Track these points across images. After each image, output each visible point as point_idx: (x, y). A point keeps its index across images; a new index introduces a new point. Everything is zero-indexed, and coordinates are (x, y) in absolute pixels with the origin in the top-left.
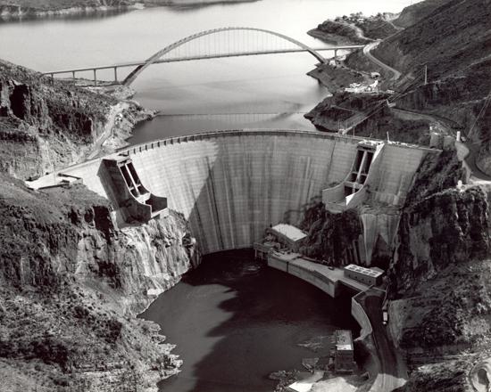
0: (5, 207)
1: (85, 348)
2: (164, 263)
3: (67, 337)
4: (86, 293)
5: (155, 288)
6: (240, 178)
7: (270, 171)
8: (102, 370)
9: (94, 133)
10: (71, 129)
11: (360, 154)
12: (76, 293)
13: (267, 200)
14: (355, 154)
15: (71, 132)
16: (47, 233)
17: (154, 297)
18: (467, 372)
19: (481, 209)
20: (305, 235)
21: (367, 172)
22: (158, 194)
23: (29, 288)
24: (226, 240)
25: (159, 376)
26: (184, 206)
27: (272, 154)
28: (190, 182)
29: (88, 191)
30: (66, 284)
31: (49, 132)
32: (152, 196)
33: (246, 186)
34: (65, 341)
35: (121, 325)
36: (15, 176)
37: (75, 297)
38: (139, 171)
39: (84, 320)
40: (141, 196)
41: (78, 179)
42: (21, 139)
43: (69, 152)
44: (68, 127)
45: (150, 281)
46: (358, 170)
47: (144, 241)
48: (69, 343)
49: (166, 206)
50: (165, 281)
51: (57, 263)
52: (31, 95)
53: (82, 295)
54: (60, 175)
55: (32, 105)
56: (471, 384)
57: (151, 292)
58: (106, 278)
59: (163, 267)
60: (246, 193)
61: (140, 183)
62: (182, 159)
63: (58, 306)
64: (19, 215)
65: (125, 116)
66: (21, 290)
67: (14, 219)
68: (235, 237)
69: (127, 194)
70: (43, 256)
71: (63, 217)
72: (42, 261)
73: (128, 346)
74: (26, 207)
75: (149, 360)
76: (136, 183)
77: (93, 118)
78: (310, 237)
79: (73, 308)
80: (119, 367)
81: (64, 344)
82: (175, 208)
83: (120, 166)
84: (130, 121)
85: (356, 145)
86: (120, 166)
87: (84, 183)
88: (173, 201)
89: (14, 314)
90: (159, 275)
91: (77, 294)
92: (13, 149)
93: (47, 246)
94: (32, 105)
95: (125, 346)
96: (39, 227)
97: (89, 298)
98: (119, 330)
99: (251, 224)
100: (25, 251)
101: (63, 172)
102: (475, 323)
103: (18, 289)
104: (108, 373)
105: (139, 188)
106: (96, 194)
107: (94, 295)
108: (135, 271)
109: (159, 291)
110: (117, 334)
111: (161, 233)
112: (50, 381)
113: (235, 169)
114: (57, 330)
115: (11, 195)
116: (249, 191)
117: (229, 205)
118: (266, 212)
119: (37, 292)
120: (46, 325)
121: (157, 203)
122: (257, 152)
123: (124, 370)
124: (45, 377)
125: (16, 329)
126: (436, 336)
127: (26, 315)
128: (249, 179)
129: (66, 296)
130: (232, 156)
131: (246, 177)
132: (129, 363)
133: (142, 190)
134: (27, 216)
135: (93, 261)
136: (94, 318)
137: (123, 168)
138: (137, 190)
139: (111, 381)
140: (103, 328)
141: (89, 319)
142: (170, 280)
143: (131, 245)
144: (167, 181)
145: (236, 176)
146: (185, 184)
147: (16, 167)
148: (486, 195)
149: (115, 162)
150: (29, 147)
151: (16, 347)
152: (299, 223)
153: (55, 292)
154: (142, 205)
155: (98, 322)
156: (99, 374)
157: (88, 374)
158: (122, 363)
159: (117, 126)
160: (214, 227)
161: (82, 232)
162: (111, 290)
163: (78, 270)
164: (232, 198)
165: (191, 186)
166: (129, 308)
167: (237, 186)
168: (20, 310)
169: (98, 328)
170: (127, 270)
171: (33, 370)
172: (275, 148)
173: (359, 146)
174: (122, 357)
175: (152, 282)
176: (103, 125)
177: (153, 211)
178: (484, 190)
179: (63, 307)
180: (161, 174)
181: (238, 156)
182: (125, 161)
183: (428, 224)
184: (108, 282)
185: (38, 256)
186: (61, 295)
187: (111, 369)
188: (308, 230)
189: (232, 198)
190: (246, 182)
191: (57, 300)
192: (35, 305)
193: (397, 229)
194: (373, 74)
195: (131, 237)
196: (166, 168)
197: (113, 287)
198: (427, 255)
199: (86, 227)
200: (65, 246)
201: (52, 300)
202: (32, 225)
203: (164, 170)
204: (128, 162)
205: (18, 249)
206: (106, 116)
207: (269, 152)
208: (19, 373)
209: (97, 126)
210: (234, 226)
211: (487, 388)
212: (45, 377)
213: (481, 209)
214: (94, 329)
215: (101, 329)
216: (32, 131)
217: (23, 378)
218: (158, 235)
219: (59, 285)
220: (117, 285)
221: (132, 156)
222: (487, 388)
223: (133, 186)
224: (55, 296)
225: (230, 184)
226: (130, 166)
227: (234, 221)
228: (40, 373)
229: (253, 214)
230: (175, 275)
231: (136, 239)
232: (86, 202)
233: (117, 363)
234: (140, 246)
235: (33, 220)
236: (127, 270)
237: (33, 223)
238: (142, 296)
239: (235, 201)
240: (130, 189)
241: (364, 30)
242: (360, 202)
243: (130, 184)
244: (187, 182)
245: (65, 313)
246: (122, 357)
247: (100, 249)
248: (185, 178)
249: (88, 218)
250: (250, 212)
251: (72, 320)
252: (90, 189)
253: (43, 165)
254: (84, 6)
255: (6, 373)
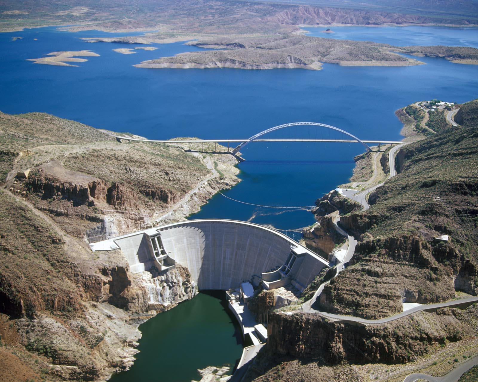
21: (291, 267)
26: (188, 264)
32: (168, 257)
38: (163, 240)
46: (287, 264)
55: (118, 195)
61: (163, 248)
71: (98, 271)
76: (160, 248)
81: (57, 349)
94: (118, 195)
96: (72, 281)
133: (163, 252)
140: (92, 339)
223: (157, 250)
242: (95, 367)
254: (278, 63)
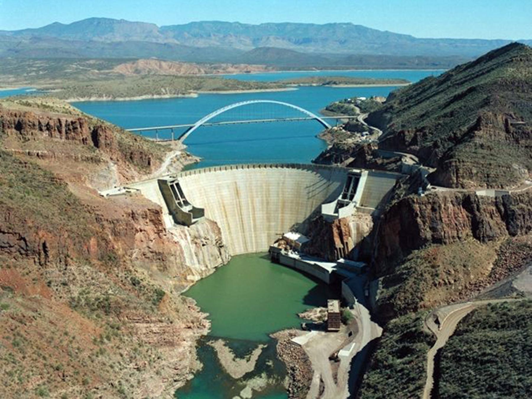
0: (81, 205)
1: (135, 305)
2: (201, 257)
3: (122, 296)
4: (140, 270)
5: (193, 275)
6: (260, 198)
7: (283, 194)
8: (148, 322)
9: (153, 168)
10: (135, 163)
11: (350, 179)
12: (131, 268)
13: (280, 215)
14: (346, 179)
15: (135, 165)
16: (112, 225)
17: (193, 281)
18: (424, 318)
19: (438, 209)
20: (308, 240)
22: (198, 206)
23: (95, 261)
24: (249, 244)
25: (192, 333)
27: (284, 181)
28: (222, 200)
29: (145, 198)
30: (124, 261)
31: (118, 160)
32: (193, 207)
33: (265, 204)
34: (120, 298)
35: (164, 293)
36: (90, 186)
37: (131, 271)
39: (137, 288)
40: (184, 207)
41: (138, 190)
42: (97, 161)
43: (133, 177)
44: (133, 162)
45: (190, 269)
46: (348, 191)
47: (186, 239)
48: (123, 300)
49: (203, 215)
50: (201, 270)
51: (119, 247)
52: (105, 132)
53: (137, 271)
54: (124, 188)
56: (426, 324)
57: (189, 278)
58: (156, 264)
59: (200, 260)
60: (265, 209)
61: (184, 197)
62: (217, 183)
63: (117, 276)
64: (91, 212)
65: (178, 160)
66: (90, 263)
67: (88, 214)
68: (257, 242)
69: (174, 205)
70: (108, 240)
71: (125, 215)
72: (107, 242)
73: (169, 309)
74: (98, 207)
75: (185, 320)
76: (182, 197)
77: (153, 156)
78: (312, 240)
79: (129, 279)
80: (161, 321)
82: (211, 218)
83: (169, 184)
84: (181, 163)
85: (347, 173)
86: (169, 184)
87: (142, 193)
88: (209, 213)
89: (83, 278)
90: (197, 266)
91: (133, 270)
92: (90, 168)
93: (112, 235)
95: (167, 308)
97: (141, 273)
98: (163, 296)
99: (268, 233)
100: (94, 235)
101: (127, 186)
102: (434, 292)
103: (88, 261)
104: (152, 325)
105: (184, 201)
106: (150, 201)
107: (146, 273)
108: (178, 261)
109: (197, 278)
110: (161, 299)
111: (199, 234)
112: (107, 325)
113: (257, 192)
114: (115, 291)
115: (86, 198)
116: (267, 208)
117: (251, 219)
118: (280, 223)
119: (102, 265)
120: (106, 287)
121: (199, 212)
122: (273, 179)
123: (164, 324)
124: (103, 323)
125: (84, 289)
126: (403, 302)
127: (92, 279)
128: (267, 200)
129: (123, 270)
130: (254, 182)
131: (265, 199)
132: (169, 319)
133: (186, 203)
134: (97, 213)
135: (147, 250)
136: (144, 287)
137: (172, 186)
138: (182, 203)
139: (154, 331)
141: (141, 287)
142: (205, 271)
143: (176, 241)
144: (206, 199)
145: (257, 197)
146: (219, 201)
147: (92, 181)
148: (441, 199)
149: (166, 181)
150: (103, 166)
151: (83, 301)
152: (304, 231)
153: (115, 266)
154: (186, 213)
155: (147, 290)
156: (145, 325)
157: (137, 324)
158: (163, 318)
159: (171, 165)
160: (240, 234)
161: (139, 227)
162: (159, 272)
163: (134, 255)
164: (254, 214)
165: (223, 203)
166: (173, 287)
167: (258, 204)
168: (87, 275)
169: (147, 294)
170: (172, 258)
171: (95, 317)
172: (287, 176)
173: (349, 174)
174: (163, 315)
175: (191, 271)
176: (161, 163)
177: (194, 218)
178: (440, 195)
179: (121, 277)
180: (200, 193)
181: (259, 182)
182: (173, 182)
183: (397, 221)
184: (157, 266)
185: (104, 239)
186: (120, 269)
187: (154, 322)
188: (310, 236)
189: (254, 214)
190: (265, 201)
191: (117, 272)
192: (99, 273)
193: (377, 233)
194: (364, 133)
195: (175, 235)
196: (204, 189)
197: (160, 270)
198: (397, 245)
199: (142, 224)
200: (125, 236)
201: (113, 272)
202: (101, 219)
203: (203, 191)
204: (176, 182)
205: (88, 232)
206: (163, 158)
207: (283, 179)
208: (83, 317)
209: (156, 163)
210: (256, 240)
211: (439, 327)
212: (103, 323)
213: (438, 209)
214: (144, 294)
215: (150, 294)
216: (105, 157)
217: (86, 321)
218: (197, 236)
219: (119, 261)
220: (164, 269)
221: (179, 179)
222: (439, 327)
223: (179, 199)
224: (116, 269)
225: (252, 203)
226: (177, 185)
227: (255, 231)
228: (100, 319)
229: (270, 225)
230: (209, 267)
231: (179, 237)
232: (143, 206)
233: (160, 318)
234: (183, 243)
235: (103, 216)
236: (172, 258)
237: (102, 218)
238: (183, 280)
239: (256, 215)
240: (177, 202)
241: (360, 108)
243: (177, 198)
244: (220, 200)
245: (122, 281)
246: (163, 315)
247: (152, 241)
248: (219, 197)
249: (145, 216)
250: (268, 224)
251: (127, 287)
252: (146, 197)
253: (112, 181)
255: (73, 316)
